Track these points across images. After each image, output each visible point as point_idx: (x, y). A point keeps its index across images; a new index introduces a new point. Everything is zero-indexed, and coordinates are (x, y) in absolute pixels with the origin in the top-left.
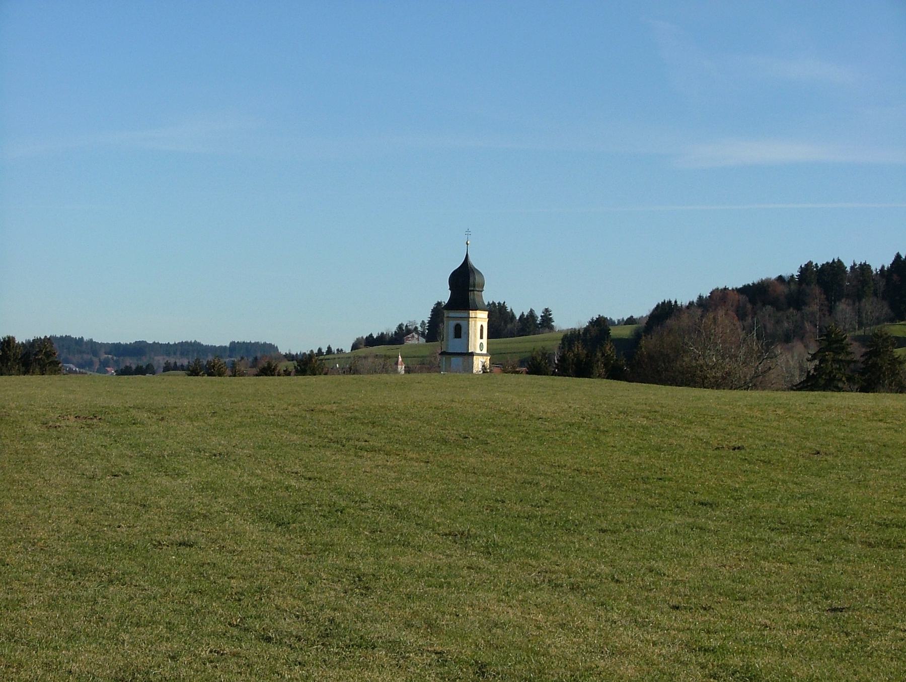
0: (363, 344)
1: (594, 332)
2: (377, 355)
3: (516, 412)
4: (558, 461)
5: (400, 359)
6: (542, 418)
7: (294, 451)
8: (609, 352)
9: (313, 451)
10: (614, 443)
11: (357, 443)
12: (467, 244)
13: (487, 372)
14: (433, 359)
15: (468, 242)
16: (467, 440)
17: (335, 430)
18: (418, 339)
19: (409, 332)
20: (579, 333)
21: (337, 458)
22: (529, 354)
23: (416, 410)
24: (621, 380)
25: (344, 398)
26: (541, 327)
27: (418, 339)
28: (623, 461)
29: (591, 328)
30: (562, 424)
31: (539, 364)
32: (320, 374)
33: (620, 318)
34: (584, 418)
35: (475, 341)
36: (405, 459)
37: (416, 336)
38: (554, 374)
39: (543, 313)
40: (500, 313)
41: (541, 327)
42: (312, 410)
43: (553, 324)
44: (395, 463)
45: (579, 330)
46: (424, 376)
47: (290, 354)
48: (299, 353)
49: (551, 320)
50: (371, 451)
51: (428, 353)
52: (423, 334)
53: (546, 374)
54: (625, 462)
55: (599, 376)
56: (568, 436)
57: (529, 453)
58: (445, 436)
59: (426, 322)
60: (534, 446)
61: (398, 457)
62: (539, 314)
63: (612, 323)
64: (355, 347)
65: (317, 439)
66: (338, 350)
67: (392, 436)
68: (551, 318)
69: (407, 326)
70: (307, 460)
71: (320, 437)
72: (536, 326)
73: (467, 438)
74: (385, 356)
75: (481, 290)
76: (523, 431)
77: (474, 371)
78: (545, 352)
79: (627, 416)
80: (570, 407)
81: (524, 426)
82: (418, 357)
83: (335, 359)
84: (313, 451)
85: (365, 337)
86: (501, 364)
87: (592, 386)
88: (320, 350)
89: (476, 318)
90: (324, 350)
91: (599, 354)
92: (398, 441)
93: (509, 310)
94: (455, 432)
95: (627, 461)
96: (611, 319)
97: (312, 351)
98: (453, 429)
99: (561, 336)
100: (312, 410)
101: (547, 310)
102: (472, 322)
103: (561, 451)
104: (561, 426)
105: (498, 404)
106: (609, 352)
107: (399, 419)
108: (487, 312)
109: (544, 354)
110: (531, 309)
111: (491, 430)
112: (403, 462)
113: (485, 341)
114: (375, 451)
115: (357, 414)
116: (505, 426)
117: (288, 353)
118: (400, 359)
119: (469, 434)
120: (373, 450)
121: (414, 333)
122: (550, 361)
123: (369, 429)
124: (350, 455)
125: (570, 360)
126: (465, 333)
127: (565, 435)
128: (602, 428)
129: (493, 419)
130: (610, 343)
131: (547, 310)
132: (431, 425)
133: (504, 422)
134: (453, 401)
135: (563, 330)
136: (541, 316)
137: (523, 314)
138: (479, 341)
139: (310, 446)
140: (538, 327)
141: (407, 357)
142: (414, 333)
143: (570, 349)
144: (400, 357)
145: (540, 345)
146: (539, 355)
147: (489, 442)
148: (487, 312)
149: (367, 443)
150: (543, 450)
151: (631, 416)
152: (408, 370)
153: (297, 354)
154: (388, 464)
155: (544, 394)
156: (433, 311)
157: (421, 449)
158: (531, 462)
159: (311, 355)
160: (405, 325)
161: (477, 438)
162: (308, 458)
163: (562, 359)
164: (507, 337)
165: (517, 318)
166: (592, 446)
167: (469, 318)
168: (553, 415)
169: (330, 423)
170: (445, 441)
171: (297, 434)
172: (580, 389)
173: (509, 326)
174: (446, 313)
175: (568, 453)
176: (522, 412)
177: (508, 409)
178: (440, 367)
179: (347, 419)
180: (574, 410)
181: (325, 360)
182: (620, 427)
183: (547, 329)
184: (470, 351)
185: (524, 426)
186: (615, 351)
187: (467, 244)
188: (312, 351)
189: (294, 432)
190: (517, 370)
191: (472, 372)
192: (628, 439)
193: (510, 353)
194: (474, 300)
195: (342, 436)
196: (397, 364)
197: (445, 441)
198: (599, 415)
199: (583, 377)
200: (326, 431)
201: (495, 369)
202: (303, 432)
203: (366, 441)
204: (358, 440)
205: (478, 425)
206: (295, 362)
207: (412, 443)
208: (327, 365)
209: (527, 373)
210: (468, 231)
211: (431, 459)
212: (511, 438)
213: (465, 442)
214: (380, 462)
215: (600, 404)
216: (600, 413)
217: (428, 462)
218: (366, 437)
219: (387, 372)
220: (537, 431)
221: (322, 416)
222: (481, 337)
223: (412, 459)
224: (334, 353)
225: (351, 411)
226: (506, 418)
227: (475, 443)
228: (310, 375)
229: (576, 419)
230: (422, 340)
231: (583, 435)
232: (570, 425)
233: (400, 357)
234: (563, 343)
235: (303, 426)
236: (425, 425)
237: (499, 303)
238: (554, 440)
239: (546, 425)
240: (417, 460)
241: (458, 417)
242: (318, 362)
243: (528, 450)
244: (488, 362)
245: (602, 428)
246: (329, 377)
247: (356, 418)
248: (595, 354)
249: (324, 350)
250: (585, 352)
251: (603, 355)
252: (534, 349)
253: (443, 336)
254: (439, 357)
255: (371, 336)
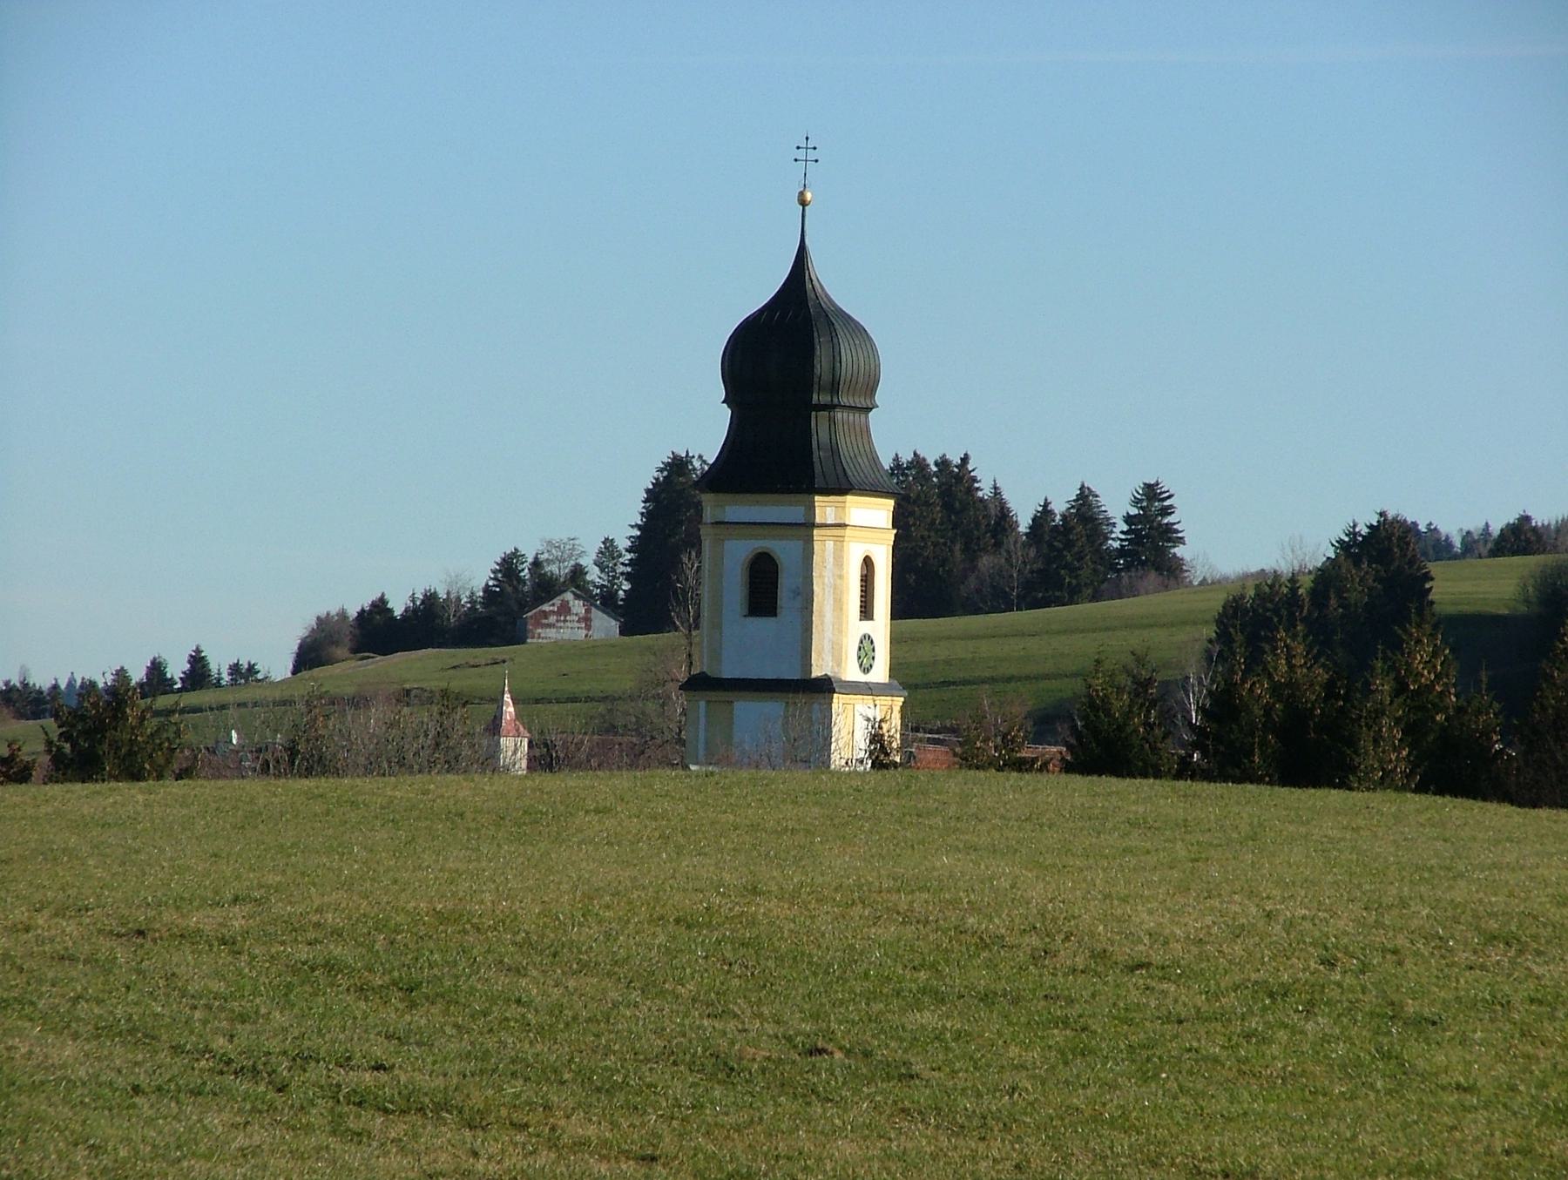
0: (348, 644)
1: (1360, 586)
2: (408, 692)
3: (1035, 941)
4: (1223, 1153)
5: (509, 709)
6: (1146, 965)
7: (66, 1111)
8: (1428, 676)
9: (148, 1112)
10: (1466, 1073)
11: (339, 1075)
12: (803, 203)
13: (895, 765)
14: (651, 707)
15: (809, 196)
16: (822, 1062)
17: (243, 1018)
18: (587, 620)
19: (546, 588)
20: (1294, 590)
21: (257, 1140)
22: (1078, 685)
23: (595, 930)
24: (1485, 799)
25: (273, 879)
26: (1127, 567)
27: (587, 620)
28: (1507, 1153)
29: (1346, 565)
30: (1236, 988)
31: (1120, 728)
32: (160, 777)
33: (1474, 525)
34: (1330, 963)
35: (839, 627)
36: (553, 1144)
37: (578, 607)
38: (1185, 771)
39: (1136, 502)
40: (947, 506)
41: (1127, 567)
42: (141, 933)
43: (1179, 551)
44: (507, 1164)
45: (1293, 580)
46: (623, 780)
47: (26, 685)
48: (63, 686)
49: (1169, 535)
50: (403, 1112)
51: (627, 684)
52: (607, 601)
53: (1151, 770)
54: (1516, 1156)
55: (1387, 782)
56: (1264, 1040)
57: (1096, 1118)
58: (723, 1044)
59: (623, 543)
60: (1114, 1086)
61: (520, 1138)
62: (1117, 506)
63: (1439, 547)
64: (310, 655)
65: (164, 1056)
66: (235, 669)
67: (490, 1043)
68: (1169, 529)
69: (537, 564)
70: (123, 1153)
71: (177, 1050)
72: (1107, 560)
73: (821, 1051)
74: (445, 694)
75: (861, 402)
76: (1065, 1022)
77: (837, 761)
78: (1145, 674)
79: (1521, 952)
80: (1269, 915)
81: (1071, 1001)
82: (589, 699)
83: (223, 707)
84: (148, 1112)
85: (353, 613)
86: (953, 731)
87: (1360, 822)
88: (156, 668)
89: (842, 526)
90: (176, 669)
91: (1383, 686)
92: (519, 1068)
93: (985, 491)
94: (770, 1028)
95: (1526, 1152)
96: (1433, 531)
97: (121, 674)
98: (760, 1016)
99: (1216, 602)
100: (141, 933)
101: (1151, 492)
102: (823, 545)
103: (1235, 1109)
104: (1230, 1000)
105: (955, 903)
106: (1428, 676)
107: (519, 971)
108: (890, 503)
109: (1142, 685)
110: (1082, 488)
111: (928, 1018)
112: (545, 1158)
113: (881, 626)
114: (421, 1110)
115: (337, 951)
116: (987, 998)
117: (16, 681)
118: (509, 709)
119: (830, 1035)
120: (410, 1105)
121: (569, 596)
122: (1167, 716)
123: (392, 1014)
124: (308, 1129)
125: (1258, 711)
126: (797, 593)
127: (1248, 1037)
128: (1411, 1007)
129: (933, 967)
130: (1432, 636)
131: (1151, 492)
132: (662, 993)
133: (982, 979)
134: (755, 891)
135: (1226, 579)
136: (1128, 519)
137: (1046, 511)
138: (856, 628)
139: (137, 1090)
140: (1113, 567)
141: (916, 686)
142: (569, 596)
143: (1255, 661)
144: (507, 698)
145: (1119, 646)
146: (1120, 690)
147: (916, 1068)
148: (890, 503)
149: (383, 1077)
150: (1156, 1107)
151: (1539, 953)
152: (544, 759)
153: (55, 687)
154: (480, 1166)
155: (1151, 860)
156: (653, 495)
157: (619, 1100)
158: (1104, 1158)
159: (119, 694)
160: (530, 560)
161: (867, 1054)
162: (127, 1140)
163: (1223, 707)
164: (977, 611)
165: (1023, 528)
166: (1372, 1087)
167: (813, 525)
168: (1195, 950)
169: (218, 986)
170: (725, 1069)
171: (75, 1036)
172: (1306, 837)
173: (986, 562)
174: (713, 507)
175: (1262, 1116)
176: (1059, 938)
177: (998, 925)
178: (682, 742)
179: (295, 971)
180: (1290, 925)
181: (182, 712)
182: (1489, 1004)
183: (1153, 575)
184: (816, 673)
185: (1071, 1001)
186: (1453, 672)
187: (803, 203)
188: (121, 674)
189: (62, 1027)
190: (1025, 754)
191: (826, 763)
192: (1528, 1057)
193: (993, 680)
194: (834, 451)
195: (274, 1045)
196: (495, 727)
197: (725, 1069)
198: (1395, 952)
199: (1316, 784)
200: (205, 1022)
201: (932, 754)
202: (102, 1031)
203: (378, 1067)
204: (345, 1062)
205: (871, 997)
206: (50, 722)
207: (583, 1076)
208: (189, 737)
209: (1068, 768)
210: (807, 145)
211: (668, 1144)
212: (1014, 1051)
213: (814, 1070)
214: (443, 1157)
215: (1404, 904)
216: (1401, 941)
217: (653, 1159)
218: (380, 1050)
219: (451, 765)
220: (1125, 1021)
221: (184, 960)
222: (866, 612)
223: (581, 1144)
224: (218, 685)
225: (311, 935)
226: (991, 965)
227: (855, 1075)
228: (117, 779)
229: (1301, 968)
230: (606, 626)
231: (1326, 1039)
232: (1271, 995)
233: (507, 698)
234: (1224, 636)
235: (99, 1002)
236: (635, 996)
237: (943, 463)
238: (1205, 1059)
239: (1164, 993)
240: (604, 1150)
241: (780, 960)
242: (152, 724)
243: (1091, 1102)
244: (896, 720)
245: (1411, 1007)
246: (202, 789)
247: (330, 967)
248: (1367, 684)
249: (176, 669)
250: (1322, 675)
251: (1401, 688)
252: (1098, 662)
253: (698, 605)
254: (679, 700)
255: (380, 606)
